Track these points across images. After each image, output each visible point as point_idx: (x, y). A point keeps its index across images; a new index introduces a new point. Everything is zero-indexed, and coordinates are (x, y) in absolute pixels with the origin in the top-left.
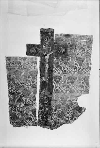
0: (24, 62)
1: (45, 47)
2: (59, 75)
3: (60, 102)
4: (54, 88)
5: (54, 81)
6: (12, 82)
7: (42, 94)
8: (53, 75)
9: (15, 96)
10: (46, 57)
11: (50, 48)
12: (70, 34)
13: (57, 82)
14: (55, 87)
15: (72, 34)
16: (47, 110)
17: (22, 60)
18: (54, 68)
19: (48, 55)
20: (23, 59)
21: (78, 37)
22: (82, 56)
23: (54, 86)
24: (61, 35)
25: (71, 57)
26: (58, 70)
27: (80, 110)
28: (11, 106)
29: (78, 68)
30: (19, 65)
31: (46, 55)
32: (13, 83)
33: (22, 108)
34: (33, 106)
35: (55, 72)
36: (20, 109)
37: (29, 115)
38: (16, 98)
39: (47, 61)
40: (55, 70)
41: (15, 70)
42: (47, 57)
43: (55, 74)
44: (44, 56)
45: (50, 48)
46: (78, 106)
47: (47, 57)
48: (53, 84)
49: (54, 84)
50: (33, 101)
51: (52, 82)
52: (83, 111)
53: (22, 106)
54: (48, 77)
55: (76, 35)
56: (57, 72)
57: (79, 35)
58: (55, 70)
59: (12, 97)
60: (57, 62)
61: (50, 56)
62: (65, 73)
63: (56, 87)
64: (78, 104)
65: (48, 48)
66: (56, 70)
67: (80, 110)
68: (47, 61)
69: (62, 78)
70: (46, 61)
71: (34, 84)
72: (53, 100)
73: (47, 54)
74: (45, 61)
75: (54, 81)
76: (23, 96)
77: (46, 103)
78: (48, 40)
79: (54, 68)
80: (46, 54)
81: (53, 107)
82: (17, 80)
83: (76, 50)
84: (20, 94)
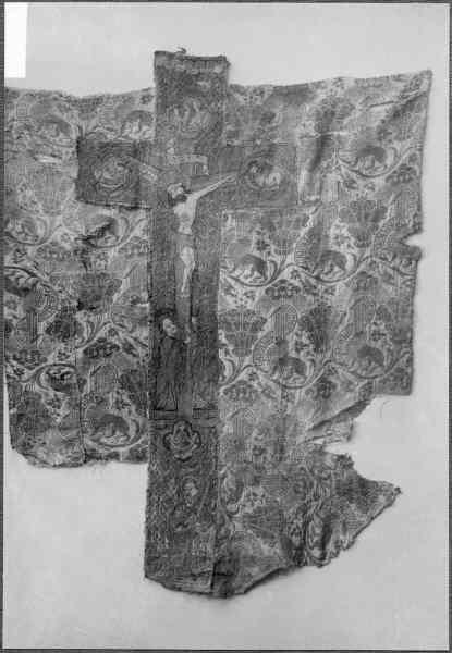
0: (83, 124)
1: (179, 153)
2: (250, 306)
3: (257, 452)
4: (224, 377)
5: (223, 339)
6: (19, 228)
7: (159, 409)
8: (219, 308)
9: (38, 303)
10: (180, 209)
11: (204, 159)
12: (309, 82)
13: (242, 346)
14: (227, 373)
15: (318, 85)
16: (194, 492)
17: (76, 112)
18: (225, 267)
19: (193, 198)
20: (82, 111)
21: (350, 91)
22: (374, 190)
23: (226, 363)
24: (262, 93)
25: (314, 208)
26: (247, 277)
27: (365, 495)
28: (18, 356)
29: (349, 258)
30: (58, 135)
31: (183, 199)
32: (26, 230)
33: (73, 367)
34: (130, 357)
35: (228, 289)
36: (62, 376)
37: (111, 401)
38: (43, 317)
39: (188, 231)
40: (229, 280)
41: (36, 166)
42: (186, 210)
43: (230, 299)
44: (172, 202)
45: (204, 159)
46: (356, 473)
47: (186, 210)
48: (221, 355)
49: (227, 352)
50: (131, 332)
51: (215, 344)
52: (382, 499)
53: (72, 359)
54: (191, 314)
55: (340, 79)
56: (239, 290)
57: (357, 81)
58: (229, 280)
59: (19, 308)
60: (243, 234)
61: (201, 203)
62: (283, 293)
63: (237, 371)
64: (355, 467)
65: (194, 159)
66: (233, 282)
67: (365, 495)
68: (185, 229)
69: (266, 320)
70: (180, 230)
71: (137, 238)
72: (222, 436)
73: (189, 192)
74: (174, 229)
75: (224, 340)
76: (80, 307)
77: (184, 457)
78: (191, 116)
79: (225, 267)
80: (180, 191)
81: (224, 476)
82: (46, 218)
83: (340, 162)
84: (63, 296)
